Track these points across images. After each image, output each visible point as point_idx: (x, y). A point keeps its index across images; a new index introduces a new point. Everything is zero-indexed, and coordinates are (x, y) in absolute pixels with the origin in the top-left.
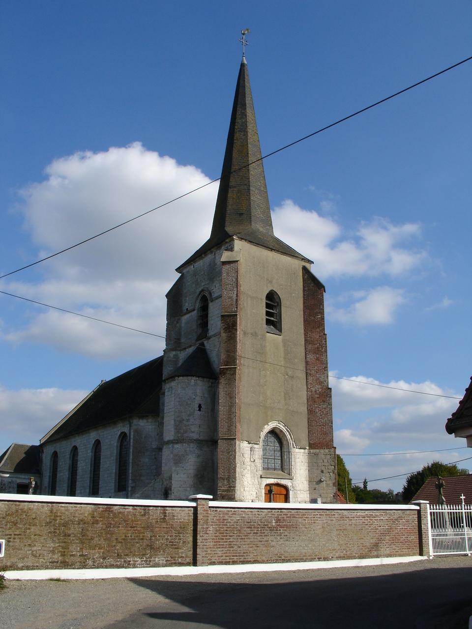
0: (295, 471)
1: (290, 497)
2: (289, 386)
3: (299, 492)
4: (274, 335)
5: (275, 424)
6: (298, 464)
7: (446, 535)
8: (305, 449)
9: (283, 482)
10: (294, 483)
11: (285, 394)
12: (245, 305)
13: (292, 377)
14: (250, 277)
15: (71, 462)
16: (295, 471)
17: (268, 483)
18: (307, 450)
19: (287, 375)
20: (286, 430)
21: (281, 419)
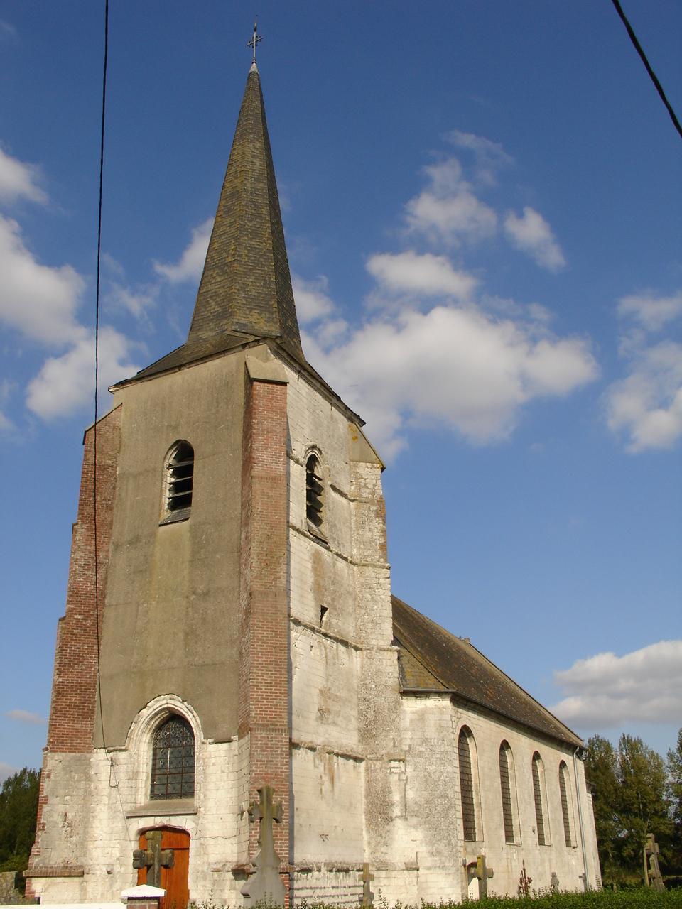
0: (205, 795)
1: (189, 871)
2: (196, 615)
3: (212, 842)
4: (174, 525)
5: (165, 702)
6: (213, 778)
7: (649, 867)
8: (230, 741)
9: (176, 822)
10: (200, 822)
11: (187, 634)
12: (123, 494)
13: (206, 594)
14: (304, 423)
15: (281, 360)
16: (205, 795)
17: (141, 827)
18: (235, 745)
19: (194, 593)
20: (186, 710)
21: (173, 688)
